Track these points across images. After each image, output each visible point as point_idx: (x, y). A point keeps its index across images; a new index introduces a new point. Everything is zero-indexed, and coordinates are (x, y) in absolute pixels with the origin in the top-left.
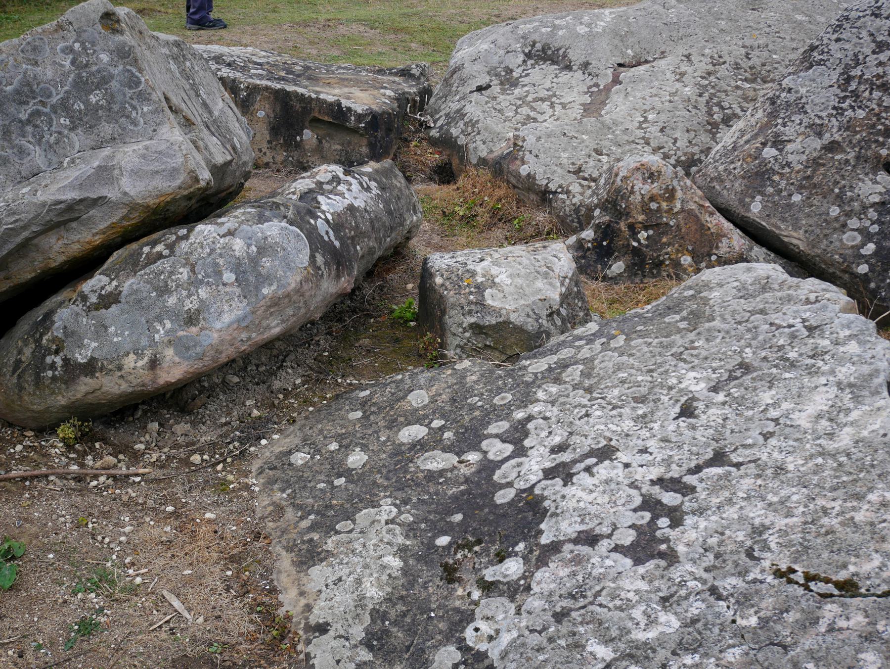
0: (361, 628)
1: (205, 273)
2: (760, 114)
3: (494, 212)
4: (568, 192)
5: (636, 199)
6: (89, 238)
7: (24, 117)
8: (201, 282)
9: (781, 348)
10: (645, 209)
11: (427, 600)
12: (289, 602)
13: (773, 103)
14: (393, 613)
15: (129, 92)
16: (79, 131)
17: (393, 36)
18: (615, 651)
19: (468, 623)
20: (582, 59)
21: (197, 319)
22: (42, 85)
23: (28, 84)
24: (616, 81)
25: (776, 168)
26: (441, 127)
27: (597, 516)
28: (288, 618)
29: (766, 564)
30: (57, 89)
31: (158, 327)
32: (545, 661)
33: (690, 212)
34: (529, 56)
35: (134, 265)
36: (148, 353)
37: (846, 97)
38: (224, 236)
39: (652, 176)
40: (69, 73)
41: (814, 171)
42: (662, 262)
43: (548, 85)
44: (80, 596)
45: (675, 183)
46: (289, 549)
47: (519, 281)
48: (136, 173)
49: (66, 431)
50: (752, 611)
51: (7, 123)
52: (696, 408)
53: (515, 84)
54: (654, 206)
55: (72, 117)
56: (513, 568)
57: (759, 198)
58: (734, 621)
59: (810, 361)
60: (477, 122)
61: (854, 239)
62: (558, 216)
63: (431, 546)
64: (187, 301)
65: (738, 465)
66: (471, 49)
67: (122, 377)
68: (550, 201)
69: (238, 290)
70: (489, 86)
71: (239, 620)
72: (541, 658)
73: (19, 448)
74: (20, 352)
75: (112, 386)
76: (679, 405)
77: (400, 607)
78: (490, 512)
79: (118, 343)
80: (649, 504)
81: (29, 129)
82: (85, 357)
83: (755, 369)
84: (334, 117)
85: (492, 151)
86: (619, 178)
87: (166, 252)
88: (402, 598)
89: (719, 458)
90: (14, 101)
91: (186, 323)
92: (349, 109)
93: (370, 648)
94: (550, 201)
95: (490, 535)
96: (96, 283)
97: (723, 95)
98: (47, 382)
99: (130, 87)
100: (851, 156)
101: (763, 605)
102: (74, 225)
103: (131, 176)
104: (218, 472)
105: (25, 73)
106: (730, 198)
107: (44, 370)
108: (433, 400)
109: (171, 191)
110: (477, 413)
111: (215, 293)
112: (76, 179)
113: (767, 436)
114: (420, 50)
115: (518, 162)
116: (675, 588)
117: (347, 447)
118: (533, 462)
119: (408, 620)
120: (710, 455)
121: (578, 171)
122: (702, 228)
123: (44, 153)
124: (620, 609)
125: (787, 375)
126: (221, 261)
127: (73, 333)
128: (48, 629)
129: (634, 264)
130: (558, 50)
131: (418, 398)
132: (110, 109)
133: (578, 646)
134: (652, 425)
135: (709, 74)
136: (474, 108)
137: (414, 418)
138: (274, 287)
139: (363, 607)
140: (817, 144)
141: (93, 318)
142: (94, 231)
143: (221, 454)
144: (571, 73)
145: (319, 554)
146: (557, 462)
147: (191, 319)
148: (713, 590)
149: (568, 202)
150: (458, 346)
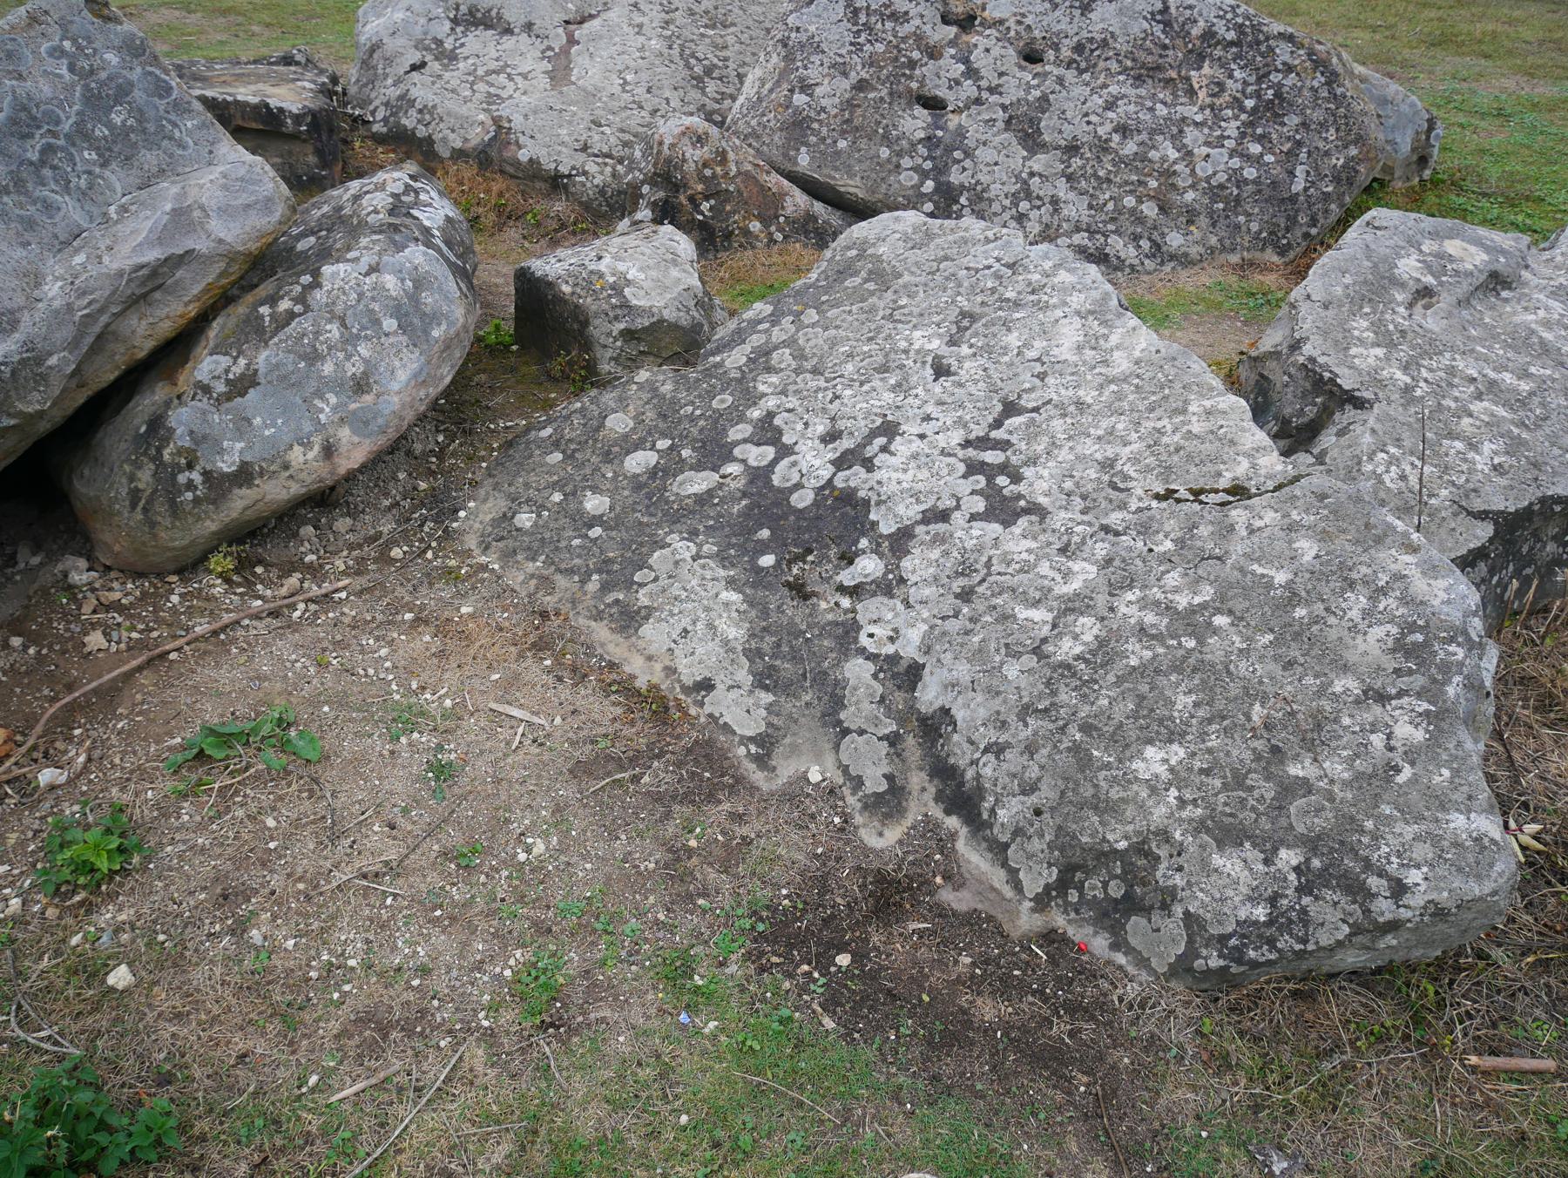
0: (744, 672)
1: (358, 324)
2: (775, 59)
3: (499, 209)
4: (585, 173)
5: (690, 167)
6: (181, 309)
7: (34, 156)
8: (358, 337)
9: (993, 290)
10: (702, 179)
11: (792, 623)
12: (644, 674)
13: (785, 46)
14: (766, 647)
15: (161, 104)
16: (114, 165)
17: (222, 20)
18: (1051, 610)
19: (858, 632)
20: (523, 20)
21: (368, 384)
22: (43, 107)
23: (24, 108)
24: (572, 41)
25: (813, 114)
26: (385, 120)
27: (931, 492)
28: (653, 687)
29: (1140, 492)
30: (64, 110)
31: (320, 405)
32: (983, 640)
33: (747, 174)
34: (455, 21)
35: (256, 332)
36: (317, 440)
37: (859, 31)
38: (367, 274)
39: (700, 140)
40: (73, 86)
41: (851, 113)
42: (732, 232)
43: (495, 55)
44: (403, 740)
45: (724, 143)
46: (598, 617)
47: (654, 273)
48: (225, 211)
49: (221, 562)
50: (1161, 536)
51: (14, 167)
52: (949, 366)
53: (452, 57)
54: (708, 172)
55: (98, 149)
56: (869, 566)
57: (803, 149)
58: (1151, 550)
59: (1032, 297)
60: (434, 107)
61: (911, 178)
62: (581, 203)
63: (759, 570)
64: (348, 365)
65: (1036, 410)
66: (382, 20)
67: (291, 477)
68: (565, 187)
69: (404, 339)
70: (423, 65)
71: (603, 711)
72: (976, 639)
73: (175, 599)
74: (132, 478)
75: (276, 491)
76: (928, 366)
77: (770, 640)
78: (798, 519)
79: (273, 436)
80: (973, 468)
81: (47, 172)
82: (233, 463)
83: (982, 316)
84: (263, 123)
85: (466, 140)
86: (666, 147)
87: (298, 308)
88: (764, 629)
89: (1010, 409)
90: (12, 135)
91: (355, 393)
92: (281, 110)
93: (766, 688)
94: (565, 187)
95: (816, 541)
96: (208, 366)
97: (692, 45)
98: (188, 509)
99: (161, 97)
100: (884, 92)
101: (1167, 528)
102: (157, 295)
103: (220, 217)
104: (430, 561)
105: (14, 92)
106: (776, 155)
107: (180, 493)
108: (638, 419)
109: (272, 228)
110: (702, 423)
111: (378, 348)
112: (150, 231)
113: (1042, 376)
114: (267, 33)
115: (513, 147)
116: (1065, 538)
117: (574, 494)
118: (808, 457)
119: (785, 648)
120: (999, 407)
121: (585, 148)
122: (764, 190)
123: (78, 205)
124: (1021, 571)
125: (1017, 315)
126: (376, 307)
127: (205, 437)
128: (399, 787)
129: (704, 240)
130: (489, 11)
131: (619, 423)
132: (144, 131)
133: (1006, 617)
134: (914, 392)
135: (667, 23)
136: (422, 90)
137: (630, 444)
138: (443, 327)
139: (733, 650)
140: (845, 84)
141: (227, 412)
142: (186, 299)
143: (421, 540)
144: (514, 38)
145: (638, 612)
146: (840, 450)
147: (360, 386)
148: (1106, 529)
149: (589, 185)
150: (611, 359)
